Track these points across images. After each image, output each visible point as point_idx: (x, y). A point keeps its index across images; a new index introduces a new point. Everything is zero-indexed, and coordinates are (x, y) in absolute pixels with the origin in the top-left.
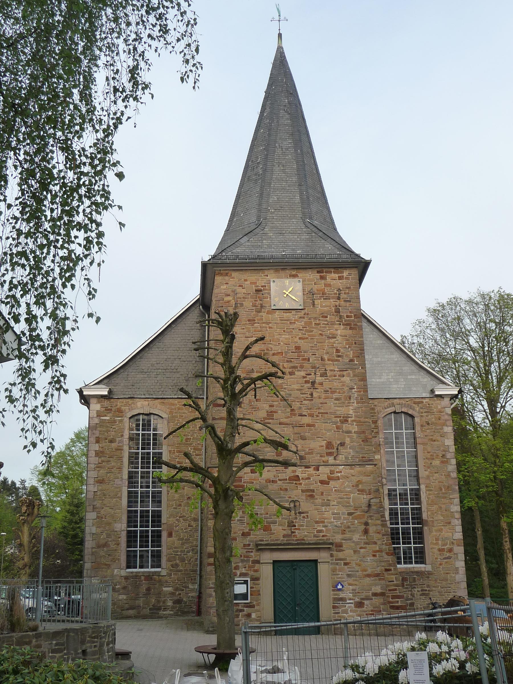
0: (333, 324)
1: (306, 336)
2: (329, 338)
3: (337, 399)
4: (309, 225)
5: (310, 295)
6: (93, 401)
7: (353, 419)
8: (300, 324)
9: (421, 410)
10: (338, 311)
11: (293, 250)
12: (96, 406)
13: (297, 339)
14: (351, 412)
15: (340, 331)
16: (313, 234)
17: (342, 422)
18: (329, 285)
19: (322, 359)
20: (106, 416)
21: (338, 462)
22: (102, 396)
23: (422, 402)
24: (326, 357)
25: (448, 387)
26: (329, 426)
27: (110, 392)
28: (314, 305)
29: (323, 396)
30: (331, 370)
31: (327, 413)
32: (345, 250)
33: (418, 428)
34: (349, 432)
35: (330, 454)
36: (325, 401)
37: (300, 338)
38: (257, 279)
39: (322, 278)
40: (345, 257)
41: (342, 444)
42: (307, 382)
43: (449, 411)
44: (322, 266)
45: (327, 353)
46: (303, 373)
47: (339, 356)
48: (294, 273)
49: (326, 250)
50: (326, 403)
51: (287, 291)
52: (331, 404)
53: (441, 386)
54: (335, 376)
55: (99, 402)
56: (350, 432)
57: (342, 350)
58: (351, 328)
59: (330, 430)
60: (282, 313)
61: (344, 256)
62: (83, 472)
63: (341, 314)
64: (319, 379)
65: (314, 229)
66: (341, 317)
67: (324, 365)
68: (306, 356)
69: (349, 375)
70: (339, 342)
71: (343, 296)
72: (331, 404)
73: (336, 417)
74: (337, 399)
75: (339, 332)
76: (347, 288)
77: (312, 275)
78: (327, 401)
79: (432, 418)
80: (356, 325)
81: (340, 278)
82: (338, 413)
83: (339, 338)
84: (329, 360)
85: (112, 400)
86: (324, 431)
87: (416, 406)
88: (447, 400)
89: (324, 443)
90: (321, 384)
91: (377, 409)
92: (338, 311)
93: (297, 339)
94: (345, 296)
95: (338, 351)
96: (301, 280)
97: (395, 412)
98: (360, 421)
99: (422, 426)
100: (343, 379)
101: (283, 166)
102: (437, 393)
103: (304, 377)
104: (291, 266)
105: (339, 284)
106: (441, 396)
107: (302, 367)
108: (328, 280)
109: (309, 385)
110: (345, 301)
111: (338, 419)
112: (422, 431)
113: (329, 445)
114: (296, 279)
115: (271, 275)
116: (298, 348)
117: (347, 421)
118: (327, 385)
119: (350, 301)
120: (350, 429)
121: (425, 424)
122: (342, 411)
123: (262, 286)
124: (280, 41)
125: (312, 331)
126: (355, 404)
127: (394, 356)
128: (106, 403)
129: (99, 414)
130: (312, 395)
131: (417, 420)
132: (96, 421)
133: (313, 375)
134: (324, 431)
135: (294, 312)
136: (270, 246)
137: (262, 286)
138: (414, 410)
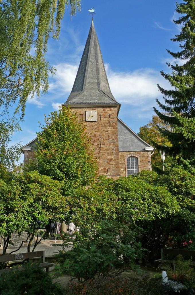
0: (107, 126)
1: (98, 131)
2: (106, 131)
3: (108, 153)
4: (100, 91)
5: (99, 116)
6: (25, 152)
7: (113, 160)
8: (96, 127)
9: (141, 156)
10: (109, 122)
11: (94, 100)
12: (27, 154)
13: (95, 132)
14: (113, 158)
15: (110, 129)
16: (102, 94)
17: (109, 161)
18: (107, 113)
19: (103, 139)
20: (30, 157)
21: (108, 175)
22: (29, 151)
23: (141, 153)
24: (104, 138)
25: (150, 148)
26: (105, 162)
27: (31, 149)
28: (101, 119)
29: (103, 152)
30: (106, 143)
31: (104, 158)
32: (112, 100)
33: (139, 162)
34: (112, 164)
35: (105, 172)
36: (104, 154)
37: (95, 132)
38: (82, 110)
39: (104, 110)
40: (112, 102)
41: (109, 169)
42: (97, 147)
43: (150, 156)
44: (104, 106)
45: (105, 137)
46: (96, 144)
47: (109, 138)
48: (94, 109)
49: (107, 101)
50: (104, 154)
51: (92, 115)
52: (106, 155)
53: (148, 147)
54: (107, 145)
55: (28, 152)
56: (112, 165)
57: (110, 136)
58: (113, 128)
59: (104, 164)
60: (90, 123)
61: (112, 103)
62: (144, 233)
63: (110, 123)
64: (102, 146)
65: (102, 92)
66: (110, 124)
67: (104, 141)
68: (98, 138)
69: (112, 145)
70: (109, 133)
71: (111, 116)
72: (106, 155)
73: (107, 159)
74: (108, 153)
75: (109, 130)
76: (112, 114)
77: (101, 109)
78: (104, 154)
79: (144, 159)
80: (115, 127)
81: (110, 110)
82: (108, 158)
83: (109, 132)
84: (106, 139)
85: (32, 152)
86: (103, 164)
87: (138, 154)
88: (150, 153)
89: (103, 168)
90: (103, 148)
91: (125, 155)
92: (109, 122)
93: (95, 132)
94: (112, 117)
95: (109, 136)
96: (97, 111)
97: (131, 157)
98: (116, 161)
99: (141, 161)
100: (110, 146)
101: (92, 69)
102: (146, 150)
103: (97, 145)
104: (93, 106)
105: (110, 112)
106: (148, 151)
107: (96, 142)
108: (106, 111)
109: (99, 148)
110: (112, 118)
111: (108, 160)
112: (141, 163)
113: (105, 169)
114: (95, 111)
115: (86, 110)
116: (95, 135)
117: (111, 161)
118: (105, 148)
119: (113, 118)
120: (112, 163)
121: (141, 161)
122: (109, 157)
123: (83, 113)
124: (91, 30)
125: (100, 129)
126: (114, 155)
127: (132, 136)
128: (30, 153)
129: (28, 157)
130: (99, 152)
131: (139, 159)
132: (27, 159)
133: (100, 145)
134: (103, 164)
135: (94, 122)
136: (86, 99)
137: (83, 113)
138: (138, 155)
